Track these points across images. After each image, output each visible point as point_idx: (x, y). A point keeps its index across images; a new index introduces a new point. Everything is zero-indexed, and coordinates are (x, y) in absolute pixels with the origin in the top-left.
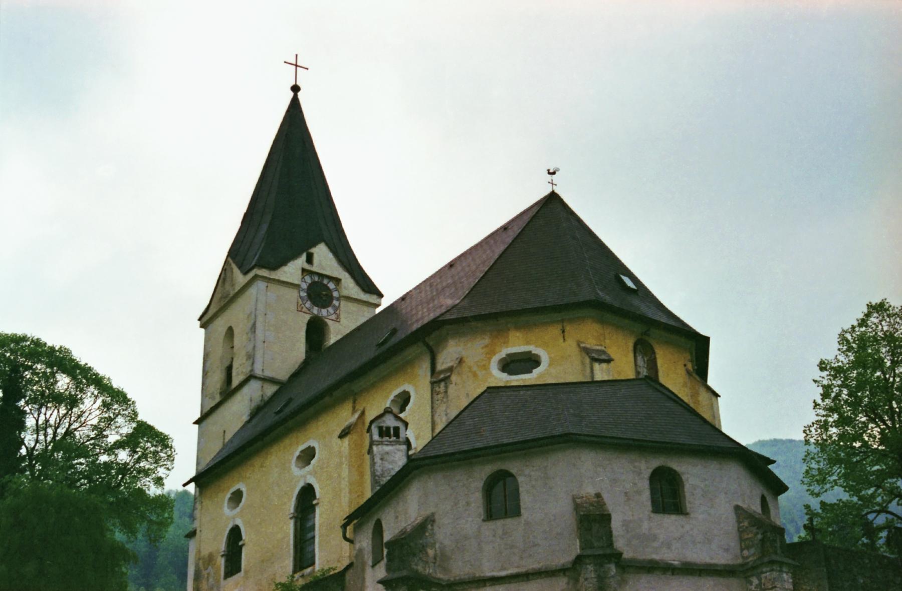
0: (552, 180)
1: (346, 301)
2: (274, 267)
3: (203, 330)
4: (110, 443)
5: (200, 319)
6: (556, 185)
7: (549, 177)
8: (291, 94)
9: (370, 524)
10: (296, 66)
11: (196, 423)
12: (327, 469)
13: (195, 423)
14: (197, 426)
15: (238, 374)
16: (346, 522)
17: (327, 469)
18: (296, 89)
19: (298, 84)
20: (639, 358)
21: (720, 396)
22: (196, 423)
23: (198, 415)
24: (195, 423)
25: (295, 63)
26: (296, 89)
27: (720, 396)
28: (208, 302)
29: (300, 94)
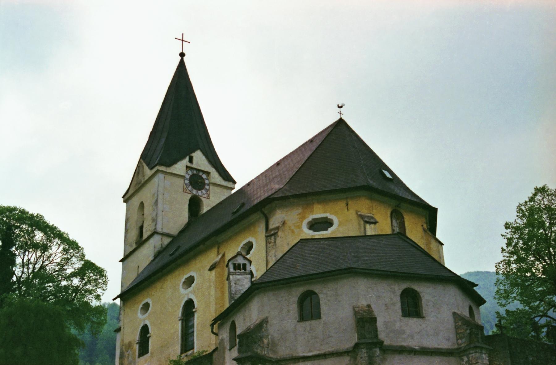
0: (340, 111)
1: (213, 186)
3: (125, 204)
5: (123, 197)
6: (343, 114)
7: (339, 109)
8: (180, 58)
10: (183, 41)
11: (121, 261)
13: (120, 261)
14: (121, 263)
15: (147, 231)
18: (182, 55)
19: (184, 52)
20: (394, 221)
21: (444, 245)
22: (121, 261)
23: (122, 257)
24: (120, 261)
26: (182, 55)
27: (444, 245)
28: (128, 187)
29: (185, 58)
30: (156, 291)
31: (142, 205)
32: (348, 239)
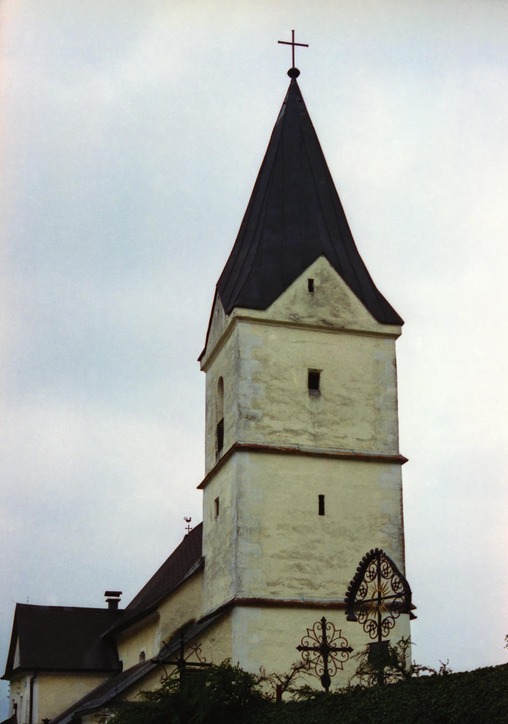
0: (189, 526)
1: (362, 336)
2: (263, 306)
3: (203, 374)
4: (191, 528)
5: (200, 359)
7: (187, 524)
8: (289, 79)
9: (196, 563)
10: (293, 44)
11: (200, 487)
12: (280, 434)
13: (199, 487)
14: (201, 491)
15: (228, 443)
16: (200, 565)
17: (280, 434)
18: (294, 73)
19: (296, 66)
20: (177, 669)
21: (121, 593)
22: (200, 487)
23: (202, 477)
24: (199, 487)
25: (296, 47)
26: (294, 73)
27: (121, 593)
28: (204, 347)
29: (299, 80)
30: (50, 677)
31: (311, 282)
32: (28, 714)
